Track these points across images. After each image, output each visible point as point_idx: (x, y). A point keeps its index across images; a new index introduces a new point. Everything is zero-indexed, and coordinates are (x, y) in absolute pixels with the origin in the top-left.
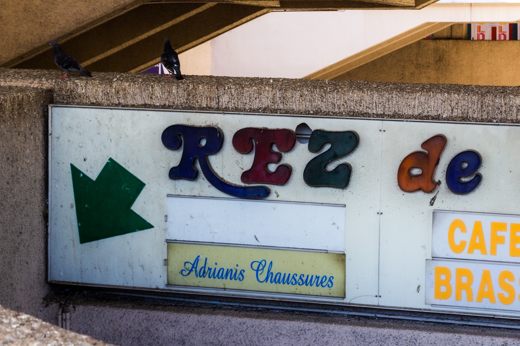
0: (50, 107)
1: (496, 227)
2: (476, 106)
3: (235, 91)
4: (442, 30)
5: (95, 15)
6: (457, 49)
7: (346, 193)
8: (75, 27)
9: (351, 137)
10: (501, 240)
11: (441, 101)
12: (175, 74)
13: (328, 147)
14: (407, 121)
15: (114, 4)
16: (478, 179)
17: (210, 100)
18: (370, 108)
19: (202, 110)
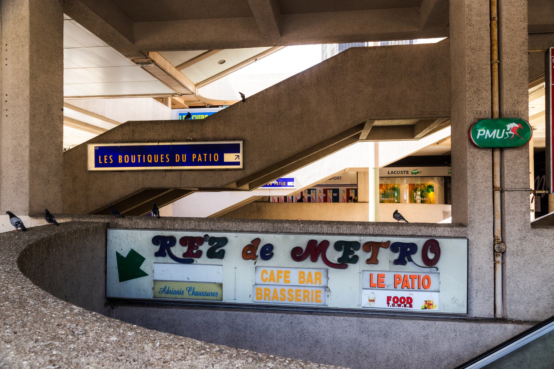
1: (279, 272)
7: (223, 260)
9: (224, 239)
10: (281, 277)
13: (216, 243)
16: (272, 254)
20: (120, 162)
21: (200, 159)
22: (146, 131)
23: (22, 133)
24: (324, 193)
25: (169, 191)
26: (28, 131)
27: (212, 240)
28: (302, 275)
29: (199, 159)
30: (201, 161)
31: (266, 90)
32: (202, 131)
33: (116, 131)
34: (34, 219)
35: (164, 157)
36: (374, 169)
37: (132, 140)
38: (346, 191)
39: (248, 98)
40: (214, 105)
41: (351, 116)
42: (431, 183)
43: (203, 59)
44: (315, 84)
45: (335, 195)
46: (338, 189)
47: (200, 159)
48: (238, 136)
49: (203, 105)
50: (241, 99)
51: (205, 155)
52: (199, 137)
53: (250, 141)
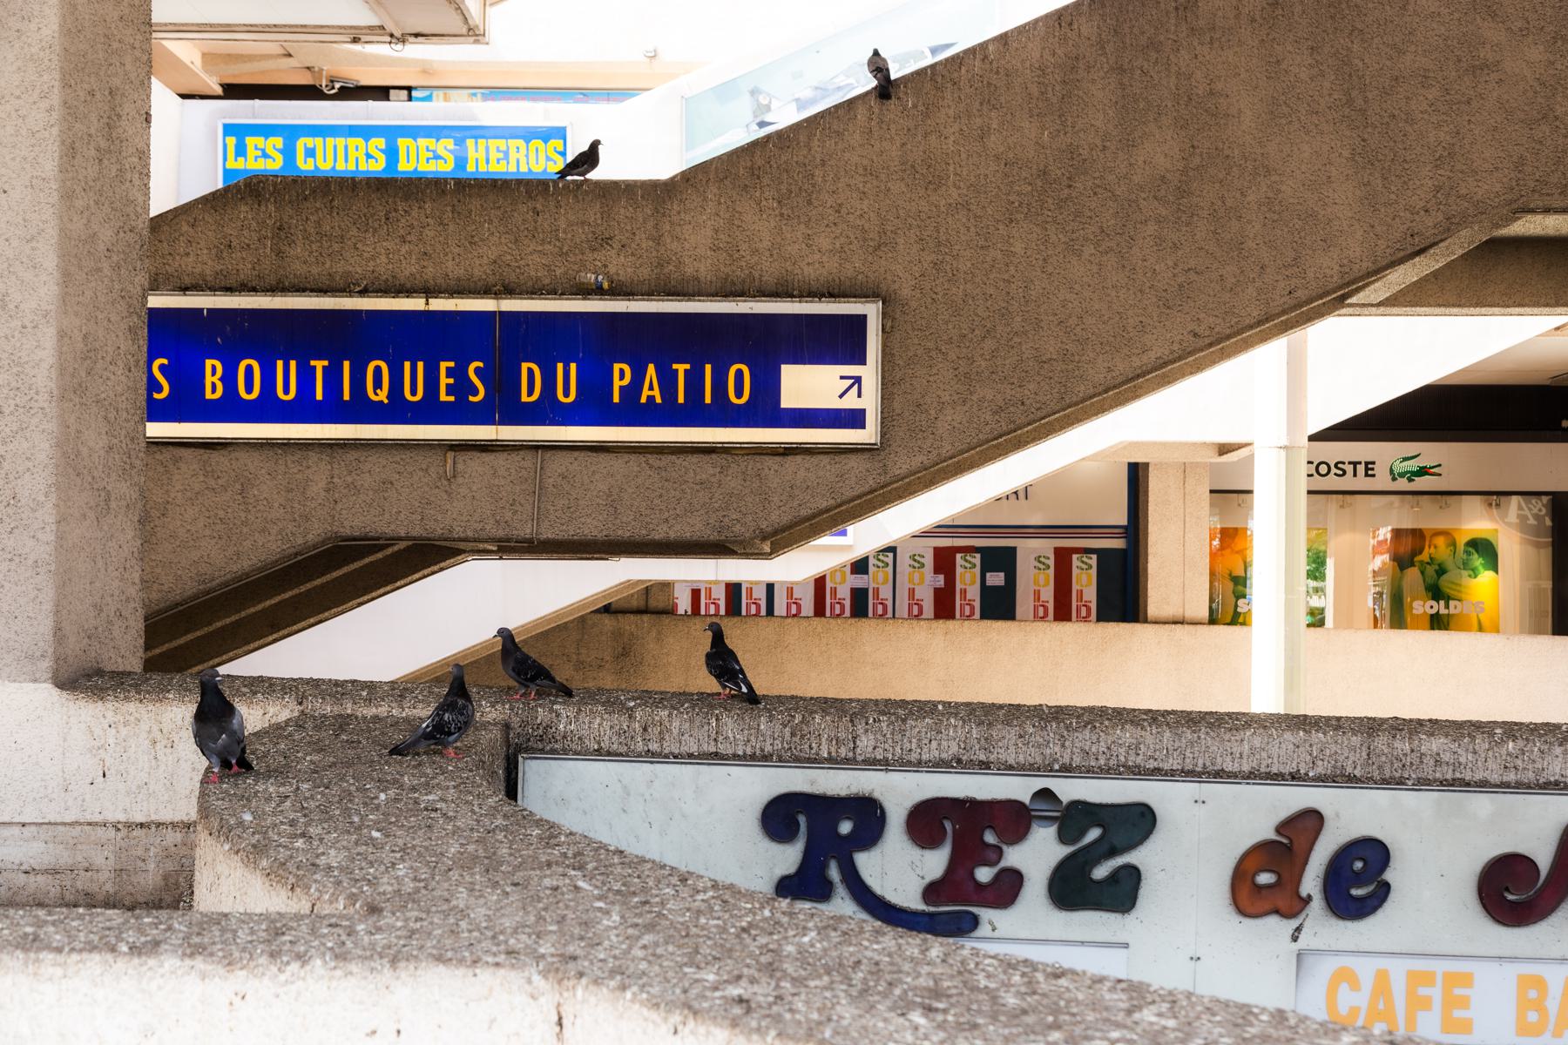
0: (520, 759)
1: (1416, 979)
2: (1358, 755)
3: (888, 726)
4: (628, 596)
5: (239, 566)
6: (659, 633)
7: (1130, 920)
8: (195, 590)
9: (1143, 814)
10: (1426, 1004)
11: (1292, 746)
12: (743, 693)
13: (1094, 834)
14: (1248, 784)
15: (283, 543)
16: (1384, 890)
17: (837, 744)
18: (1156, 760)
19: (813, 763)
20: (209, 395)
21: (651, 388)
22: (354, 232)
23: (15, 243)
24: (937, 570)
25: (389, 551)
26: (52, 232)
27: (1075, 817)
28: (1533, 994)
29: (646, 393)
30: (659, 400)
31: (1003, 39)
32: (658, 240)
33: (185, 228)
34: (82, 703)
35: (458, 373)
36: (1283, 453)
37: (272, 280)
38: (1051, 562)
39: (905, 79)
40: (365, 82)
41: (1438, 189)
42: (1476, 522)
44: (1253, 20)
45: (996, 579)
46: (1013, 550)
47: (651, 390)
48: (850, 273)
49: (303, 79)
50: (871, 83)
51: (681, 368)
52: (645, 273)
53: (914, 304)
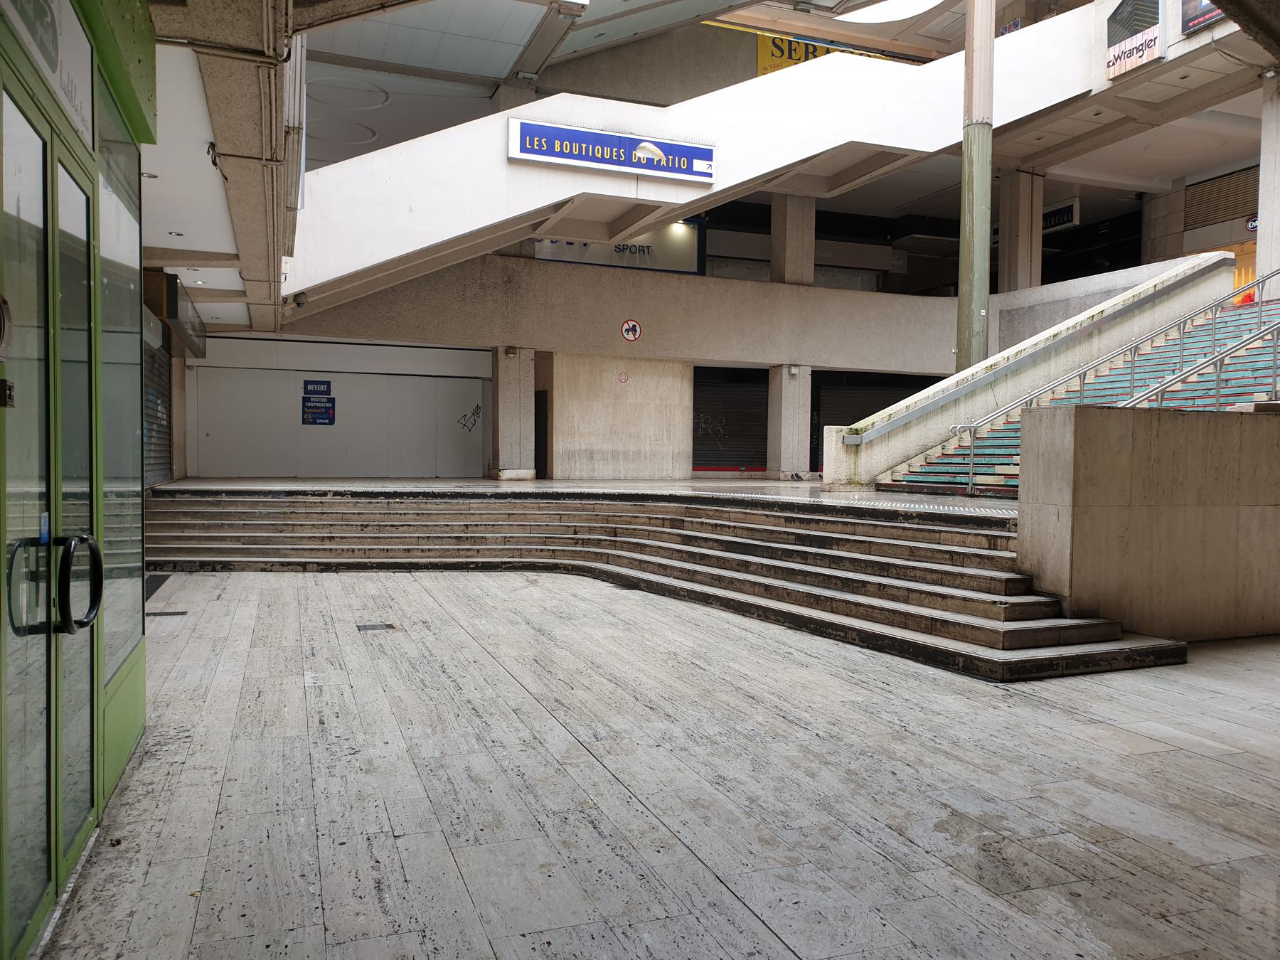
43: (846, 287)
